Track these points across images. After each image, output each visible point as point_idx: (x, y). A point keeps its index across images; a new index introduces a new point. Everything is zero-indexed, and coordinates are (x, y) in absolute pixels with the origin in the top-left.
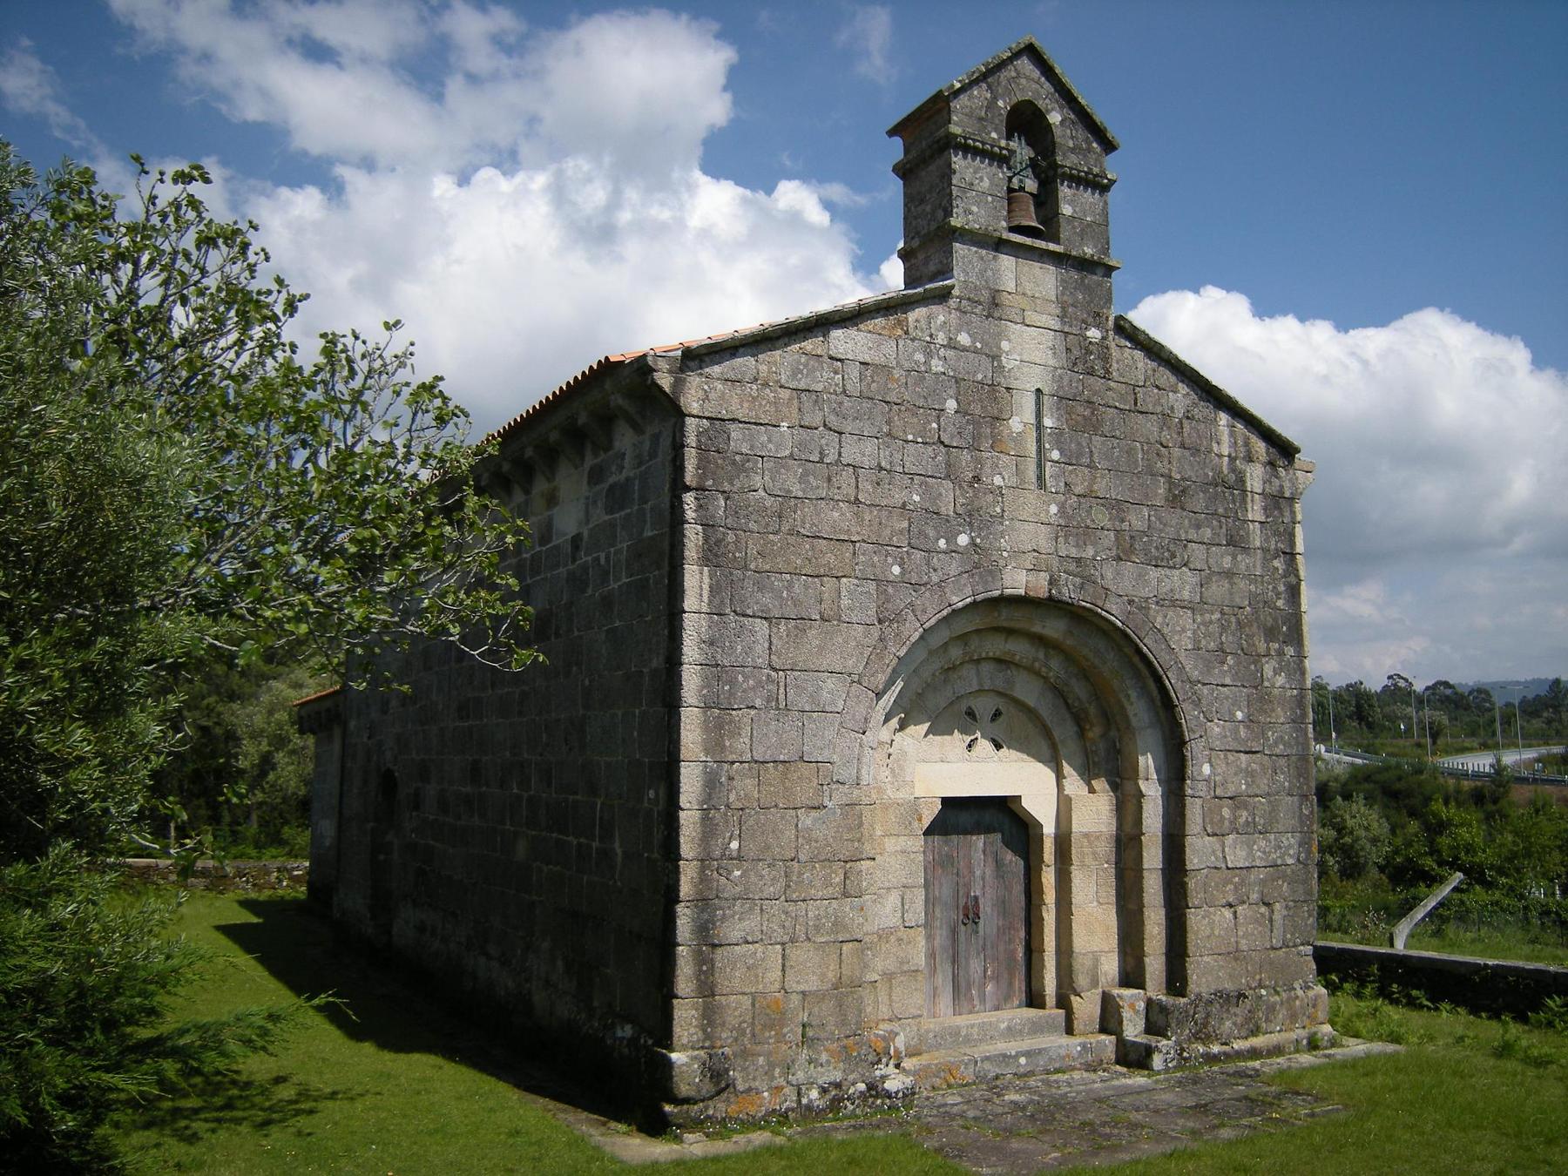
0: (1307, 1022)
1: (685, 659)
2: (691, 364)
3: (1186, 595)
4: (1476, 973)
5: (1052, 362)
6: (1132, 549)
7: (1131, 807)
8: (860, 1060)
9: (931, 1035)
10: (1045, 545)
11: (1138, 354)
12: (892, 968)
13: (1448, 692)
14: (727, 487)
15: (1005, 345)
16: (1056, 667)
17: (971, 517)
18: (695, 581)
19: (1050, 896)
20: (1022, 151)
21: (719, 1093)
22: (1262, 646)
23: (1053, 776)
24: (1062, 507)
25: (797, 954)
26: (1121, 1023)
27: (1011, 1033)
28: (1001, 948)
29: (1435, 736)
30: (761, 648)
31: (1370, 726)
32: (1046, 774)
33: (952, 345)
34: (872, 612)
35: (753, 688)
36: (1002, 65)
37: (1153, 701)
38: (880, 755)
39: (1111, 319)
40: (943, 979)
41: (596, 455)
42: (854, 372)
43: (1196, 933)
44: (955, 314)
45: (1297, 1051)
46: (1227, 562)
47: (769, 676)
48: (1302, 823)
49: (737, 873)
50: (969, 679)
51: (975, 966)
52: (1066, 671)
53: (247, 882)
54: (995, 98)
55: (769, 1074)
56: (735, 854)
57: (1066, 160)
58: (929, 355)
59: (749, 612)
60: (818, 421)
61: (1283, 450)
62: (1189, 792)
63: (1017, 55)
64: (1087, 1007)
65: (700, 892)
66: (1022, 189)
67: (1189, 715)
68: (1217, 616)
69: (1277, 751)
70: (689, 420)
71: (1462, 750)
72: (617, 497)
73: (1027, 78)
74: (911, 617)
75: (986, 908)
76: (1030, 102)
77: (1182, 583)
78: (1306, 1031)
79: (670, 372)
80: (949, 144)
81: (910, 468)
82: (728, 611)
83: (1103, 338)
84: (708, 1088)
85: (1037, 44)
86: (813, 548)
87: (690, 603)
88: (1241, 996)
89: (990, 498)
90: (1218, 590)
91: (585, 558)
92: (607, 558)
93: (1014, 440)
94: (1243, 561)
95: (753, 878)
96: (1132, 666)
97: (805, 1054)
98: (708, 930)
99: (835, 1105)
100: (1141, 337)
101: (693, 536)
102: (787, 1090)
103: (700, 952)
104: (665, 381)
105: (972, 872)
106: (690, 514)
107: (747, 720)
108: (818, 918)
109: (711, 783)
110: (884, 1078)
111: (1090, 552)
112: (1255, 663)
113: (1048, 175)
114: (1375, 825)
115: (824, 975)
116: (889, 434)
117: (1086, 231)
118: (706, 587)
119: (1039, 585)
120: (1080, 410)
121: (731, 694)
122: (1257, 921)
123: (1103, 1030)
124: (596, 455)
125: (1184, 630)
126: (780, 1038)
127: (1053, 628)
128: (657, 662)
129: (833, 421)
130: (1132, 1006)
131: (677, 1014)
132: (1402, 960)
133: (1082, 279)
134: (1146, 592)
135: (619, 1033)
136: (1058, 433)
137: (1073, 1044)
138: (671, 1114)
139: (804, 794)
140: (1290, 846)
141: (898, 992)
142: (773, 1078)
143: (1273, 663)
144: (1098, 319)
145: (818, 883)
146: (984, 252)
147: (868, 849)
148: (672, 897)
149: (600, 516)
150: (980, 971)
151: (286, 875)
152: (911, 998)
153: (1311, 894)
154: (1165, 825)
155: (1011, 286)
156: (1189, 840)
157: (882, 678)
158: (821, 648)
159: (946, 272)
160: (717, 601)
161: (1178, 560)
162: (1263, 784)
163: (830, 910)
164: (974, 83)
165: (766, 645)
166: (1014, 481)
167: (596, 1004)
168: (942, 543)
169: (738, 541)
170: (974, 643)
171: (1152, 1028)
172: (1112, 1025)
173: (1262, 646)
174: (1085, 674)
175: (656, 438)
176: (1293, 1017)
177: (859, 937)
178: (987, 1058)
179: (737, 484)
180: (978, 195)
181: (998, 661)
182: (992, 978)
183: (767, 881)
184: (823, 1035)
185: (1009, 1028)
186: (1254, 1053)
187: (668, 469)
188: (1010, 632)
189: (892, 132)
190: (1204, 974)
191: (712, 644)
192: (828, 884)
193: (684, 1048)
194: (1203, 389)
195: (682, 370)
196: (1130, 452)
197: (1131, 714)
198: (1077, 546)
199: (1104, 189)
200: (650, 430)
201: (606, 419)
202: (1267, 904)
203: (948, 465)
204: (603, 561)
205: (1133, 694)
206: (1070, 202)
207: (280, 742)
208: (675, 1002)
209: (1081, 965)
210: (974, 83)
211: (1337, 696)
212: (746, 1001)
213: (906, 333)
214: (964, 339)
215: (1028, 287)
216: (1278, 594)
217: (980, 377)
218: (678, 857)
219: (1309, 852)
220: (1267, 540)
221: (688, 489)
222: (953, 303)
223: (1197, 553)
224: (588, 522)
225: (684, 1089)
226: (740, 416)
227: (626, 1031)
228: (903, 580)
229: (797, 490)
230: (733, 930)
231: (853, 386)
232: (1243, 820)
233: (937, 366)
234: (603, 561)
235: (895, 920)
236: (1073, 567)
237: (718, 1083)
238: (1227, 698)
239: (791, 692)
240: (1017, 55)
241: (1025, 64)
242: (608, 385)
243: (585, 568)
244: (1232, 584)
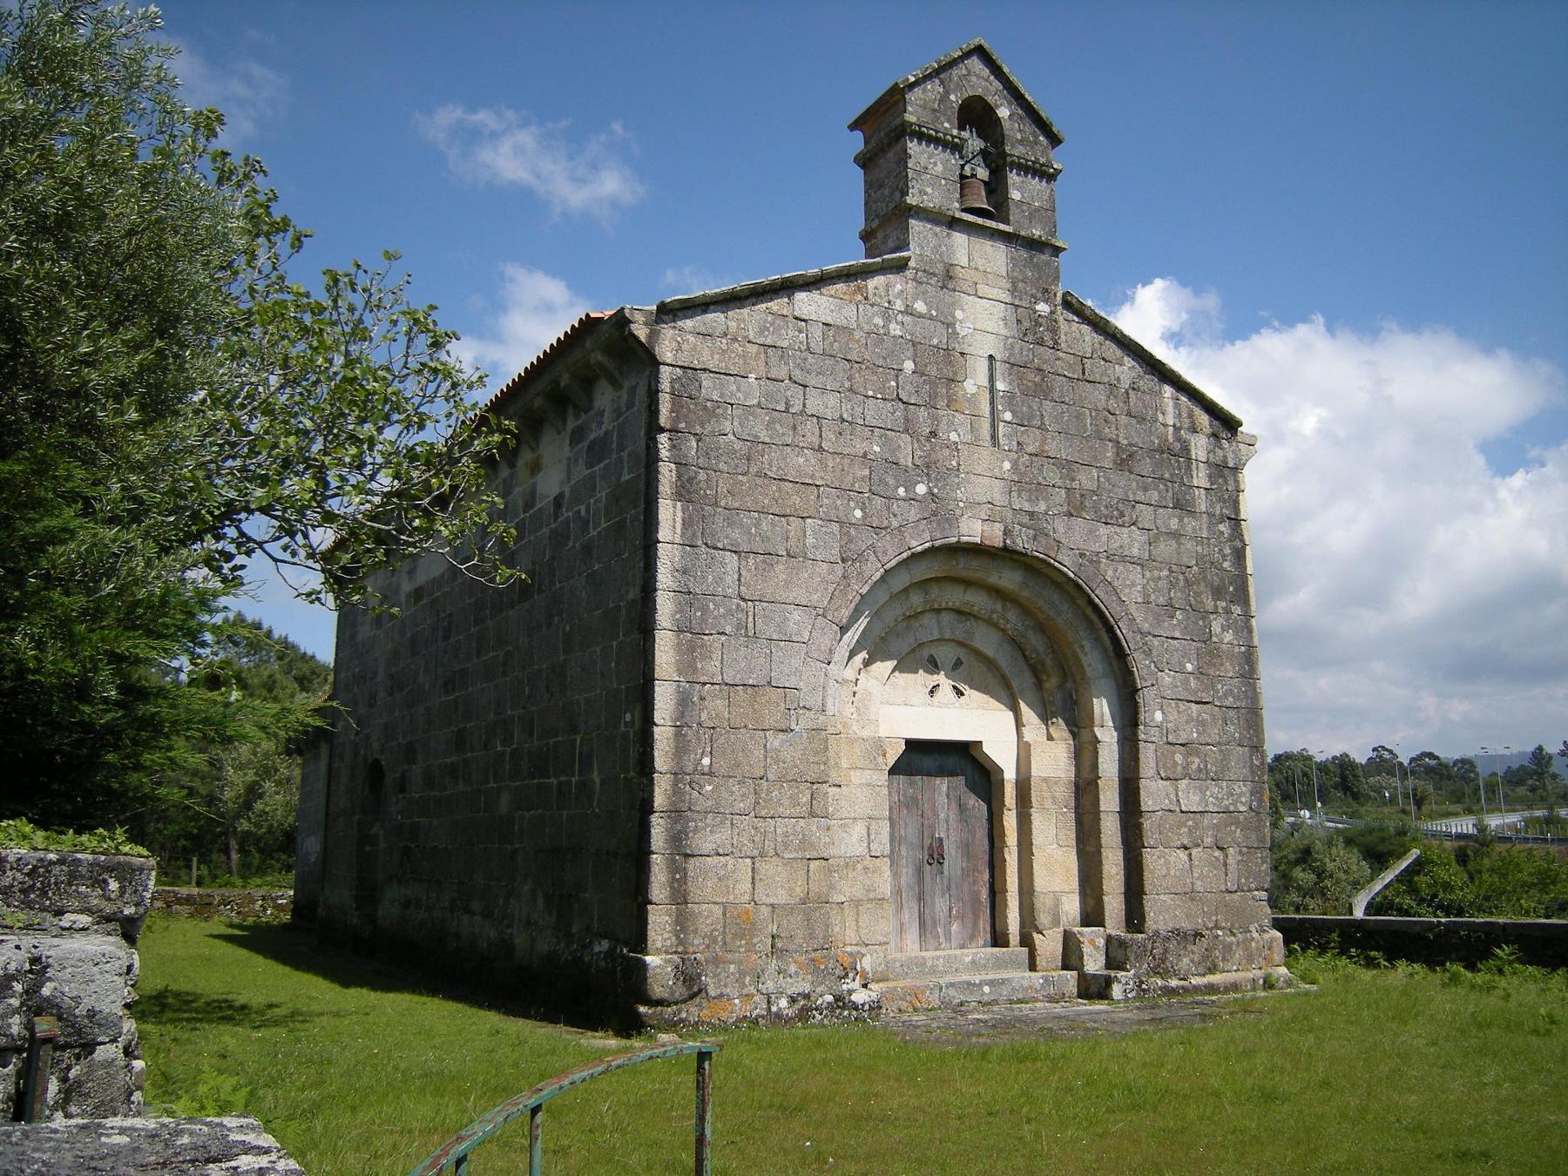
0: (1263, 963)
1: (659, 585)
2: (665, 318)
3: (1135, 552)
4: (1431, 930)
5: (1004, 332)
6: (1082, 507)
7: (1087, 755)
8: (827, 973)
10: (999, 499)
11: (1086, 328)
12: (859, 895)
13: (1433, 762)
14: (698, 430)
15: (959, 314)
16: (1013, 619)
17: (928, 468)
18: (669, 514)
19: (1012, 838)
20: (974, 143)
21: (692, 997)
22: (1209, 604)
24: (1015, 464)
25: (767, 868)
26: (1081, 958)
28: (966, 888)
29: (1419, 803)
30: (731, 579)
31: (1355, 796)
33: (909, 311)
34: (836, 551)
35: (723, 616)
36: (953, 63)
38: (845, 692)
39: (1059, 295)
40: (910, 916)
41: (577, 417)
42: (817, 332)
43: (1152, 872)
44: (911, 284)
45: (1254, 989)
46: (1174, 524)
48: (1253, 772)
49: (709, 788)
50: (930, 627)
51: (940, 905)
52: (1021, 617)
53: (232, 910)
54: (947, 93)
55: (740, 981)
56: (706, 770)
57: (1015, 150)
58: (887, 320)
59: (720, 545)
60: (783, 374)
61: (1227, 423)
62: (1142, 736)
63: (967, 55)
64: (1049, 945)
65: (673, 804)
66: (974, 176)
67: (1141, 665)
69: (1227, 703)
70: (663, 368)
71: (1447, 815)
72: (597, 451)
73: (978, 76)
74: (872, 558)
75: (951, 850)
76: (980, 97)
77: (1132, 541)
78: (1257, 959)
79: (646, 324)
80: (904, 131)
81: (870, 420)
83: (1052, 312)
84: (681, 991)
85: (986, 46)
86: (779, 490)
87: (664, 533)
88: (1198, 935)
89: (947, 452)
90: (1165, 549)
91: (567, 514)
92: (588, 511)
93: (968, 400)
94: (1190, 524)
95: (724, 794)
96: (1090, 622)
97: (774, 964)
98: (681, 840)
99: (804, 1014)
100: (1088, 313)
101: (667, 473)
102: (757, 998)
103: (674, 861)
104: (641, 332)
105: (936, 815)
106: (664, 453)
107: (718, 645)
108: (786, 835)
109: (684, 702)
110: (850, 992)
111: (1042, 507)
112: (1203, 618)
113: (997, 162)
114: (1355, 868)
116: (851, 390)
117: (1034, 214)
118: (679, 520)
119: (994, 535)
120: (1031, 376)
121: (703, 620)
122: (1211, 864)
123: (1065, 967)
124: (577, 417)
125: (1134, 584)
126: (751, 948)
127: (1009, 579)
128: (634, 593)
129: (798, 375)
130: (1092, 942)
131: (651, 918)
132: (1359, 924)
133: (1031, 258)
134: (1096, 547)
135: (597, 949)
136: (1010, 397)
137: (1036, 978)
138: (646, 1015)
139: (772, 718)
140: (1242, 794)
141: (865, 919)
142: (744, 986)
143: (1221, 620)
144: (1047, 295)
146: (938, 229)
147: (834, 776)
148: (647, 808)
149: (581, 471)
150: (946, 909)
151: (273, 897)
152: (881, 925)
153: (1264, 842)
154: (1121, 770)
155: (964, 261)
156: (1143, 783)
157: (845, 614)
158: (787, 583)
159: (904, 246)
161: (1126, 519)
162: (1214, 734)
163: (798, 829)
164: (927, 78)
166: (968, 438)
167: (574, 930)
168: (901, 491)
169: (708, 480)
170: (935, 591)
171: (1111, 963)
172: (1073, 962)
173: (1209, 604)
175: (633, 389)
176: (1250, 958)
177: (825, 855)
178: (952, 985)
179: (708, 428)
180: (932, 175)
181: (959, 612)
183: (737, 797)
184: (791, 947)
185: (973, 962)
186: (1211, 989)
187: (644, 416)
188: (968, 583)
189: (854, 126)
190: (1161, 913)
191: (685, 572)
193: (658, 952)
194: (1148, 364)
195: (657, 322)
196: (1079, 417)
198: (1030, 500)
199: (1051, 178)
200: (626, 384)
201: (587, 383)
202: (1221, 849)
203: (907, 420)
204: (583, 513)
205: (1087, 644)
206: (1019, 188)
207: (267, 772)
208: (649, 907)
209: (1042, 903)
210: (927, 78)
211: (1323, 767)
212: (718, 910)
213: (866, 298)
214: (920, 306)
215: (980, 263)
216: (1224, 556)
217: (935, 341)
218: (652, 770)
219: (1261, 801)
220: (1212, 505)
221: (662, 430)
222: (908, 273)
223: (1145, 514)
224: (569, 479)
225: (657, 991)
226: (710, 367)
227: (605, 945)
228: (866, 523)
229: (764, 436)
230: (706, 840)
231: (817, 346)
232: (1194, 766)
233: (895, 329)
234: (583, 513)
235: (861, 850)
236: (1026, 519)
237: (690, 987)
239: (759, 622)
240: (967, 55)
241: (975, 63)
242: (588, 344)
243: (567, 523)
244: (1179, 544)
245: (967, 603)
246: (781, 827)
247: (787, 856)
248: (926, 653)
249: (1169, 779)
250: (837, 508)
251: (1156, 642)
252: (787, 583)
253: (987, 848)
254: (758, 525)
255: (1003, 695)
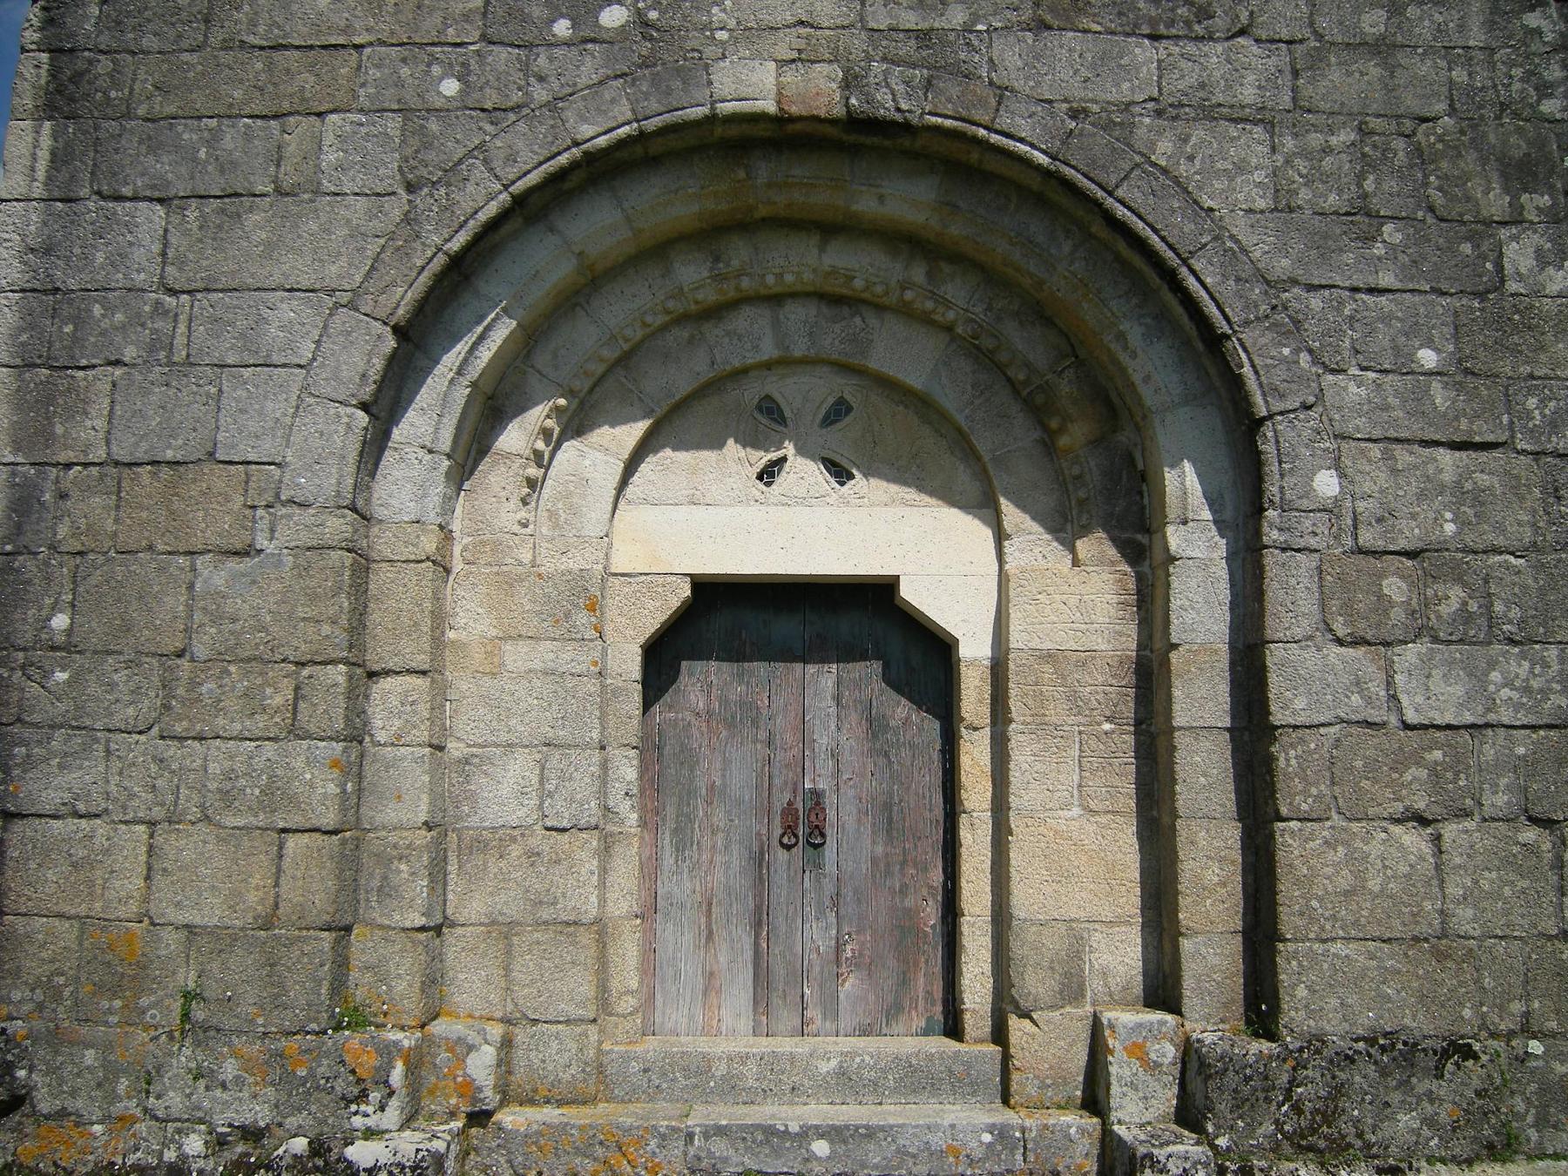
3: (1248, 94)
8: (313, 1088)
9: (635, 1066)
12: (513, 911)
16: (959, 296)
22: (1496, 202)
23: (987, 534)
25: (183, 846)
27: (846, 1082)
32: (971, 532)
34: (391, 164)
35: (123, 328)
37: (1187, 343)
40: (733, 956)
47: (158, 303)
50: (752, 336)
59: (127, 191)
62: (1272, 535)
64: (1048, 1045)
67: (1262, 359)
68: (1345, 136)
74: (480, 171)
75: (845, 817)
82: (84, 192)
86: (270, 67)
97: (185, 1057)
102: (142, 1128)
105: (805, 739)
108: (230, 775)
115: (237, 895)
118: (44, 155)
119: (821, 91)
122: (1508, 862)
125: (1241, 168)
126: (134, 1017)
127: (905, 199)
130: (1137, 1051)
139: (216, 525)
142: (114, 1097)
145: (232, 703)
158: (270, 247)
160: (63, 176)
165: (156, 248)
168: (562, 28)
170: (739, 253)
174: (1040, 313)
178: (721, 1131)
182: (856, 963)
183: (124, 695)
184: (228, 1023)
185: (842, 1073)
188: (830, 229)
192: (253, 702)
197: (1137, 378)
205: (1134, 333)
228: (466, 104)
232: (1449, 608)
236: (908, 48)
238: (1387, 319)
245: (834, 272)
246: (217, 759)
247: (231, 821)
248: (751, 392)
249: (1358, 642)
250: (400, 84)
251: (1316, 302)
252: (270, 247)
253: (939, 812)
254: (214, 138)
255: (964, 478)
